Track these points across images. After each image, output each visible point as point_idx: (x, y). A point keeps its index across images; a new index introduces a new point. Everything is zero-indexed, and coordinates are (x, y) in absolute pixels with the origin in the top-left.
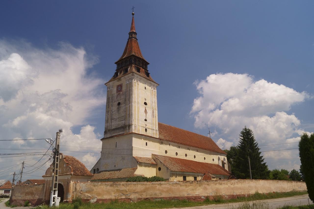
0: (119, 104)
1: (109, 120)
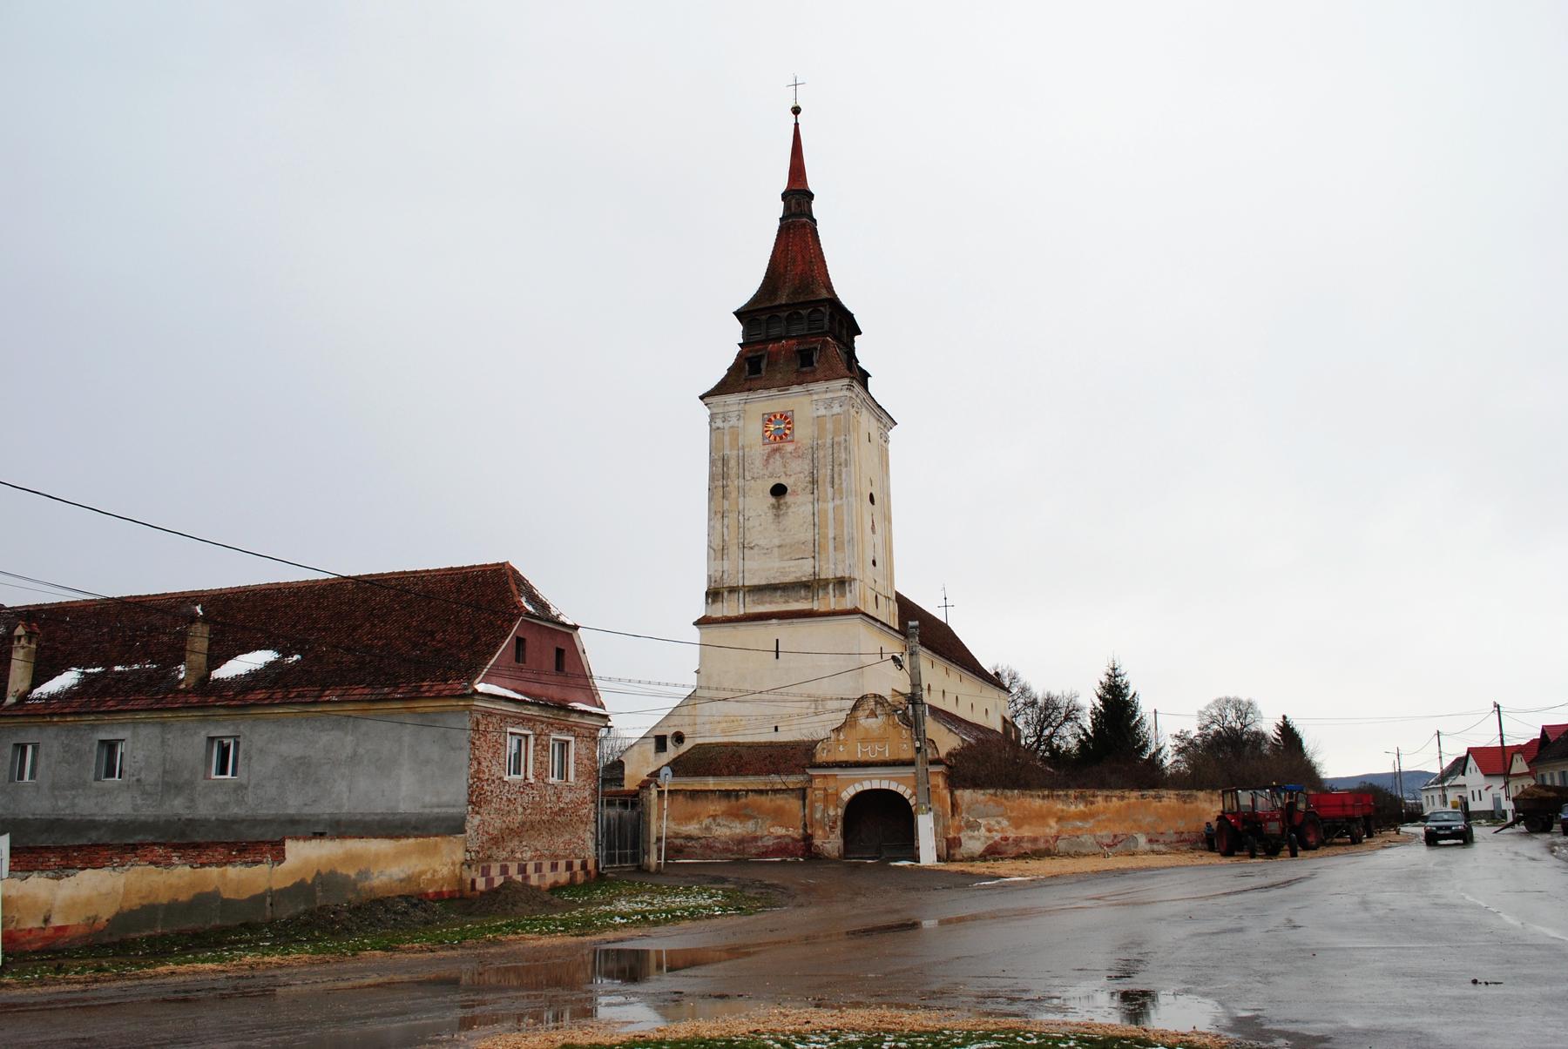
0: (779, 491)
1: (734, 550)
